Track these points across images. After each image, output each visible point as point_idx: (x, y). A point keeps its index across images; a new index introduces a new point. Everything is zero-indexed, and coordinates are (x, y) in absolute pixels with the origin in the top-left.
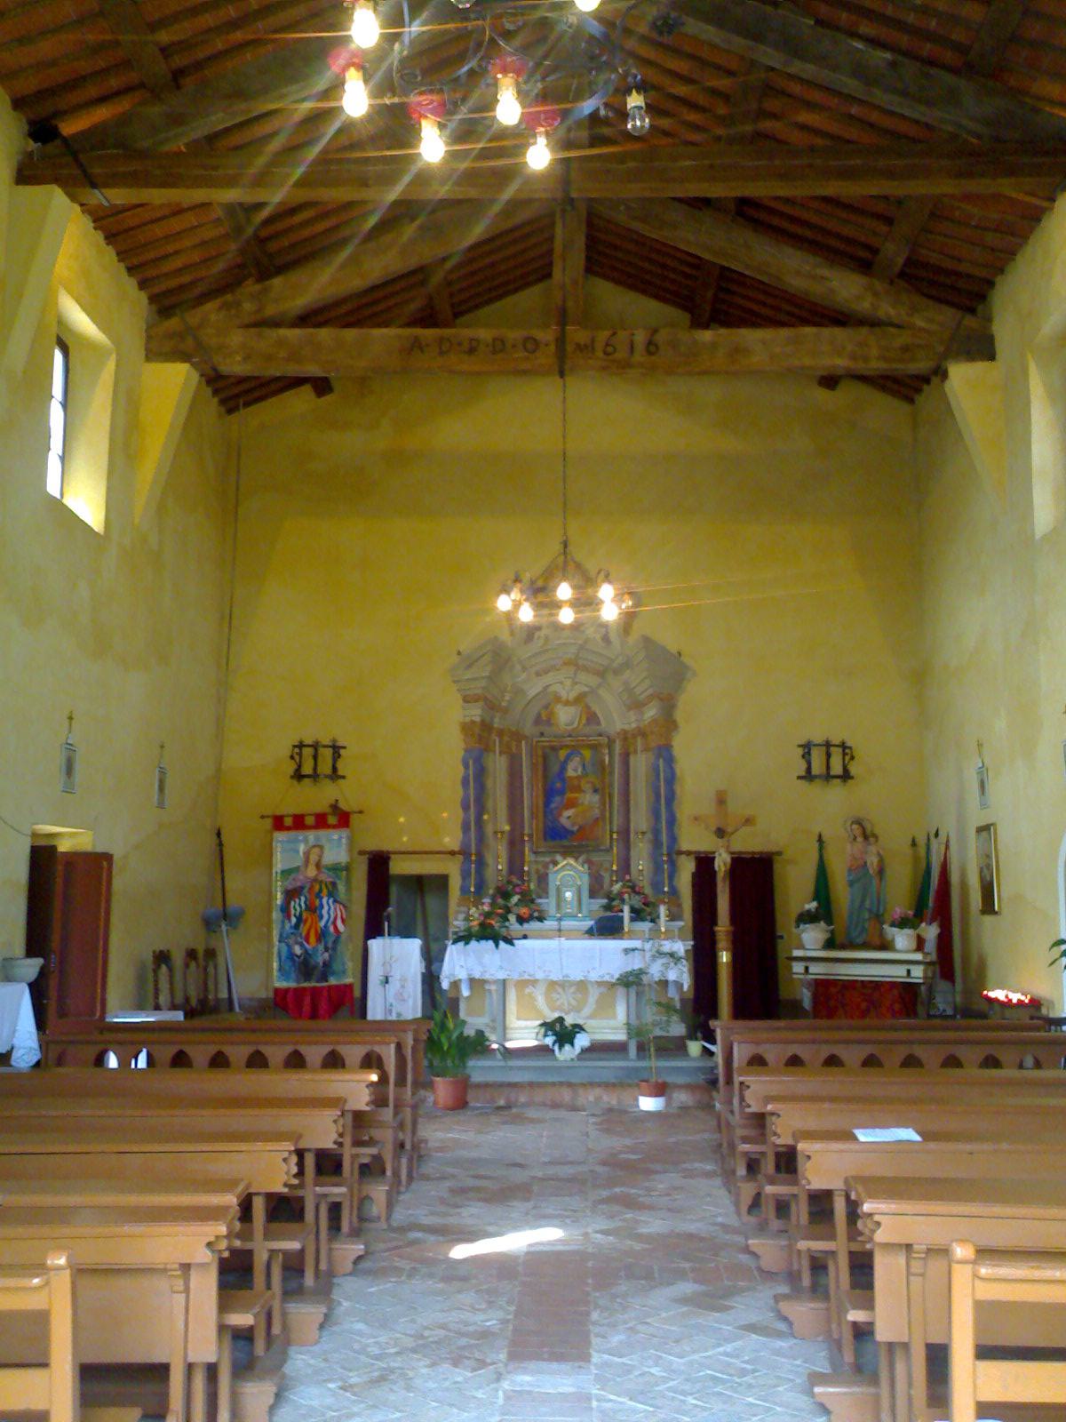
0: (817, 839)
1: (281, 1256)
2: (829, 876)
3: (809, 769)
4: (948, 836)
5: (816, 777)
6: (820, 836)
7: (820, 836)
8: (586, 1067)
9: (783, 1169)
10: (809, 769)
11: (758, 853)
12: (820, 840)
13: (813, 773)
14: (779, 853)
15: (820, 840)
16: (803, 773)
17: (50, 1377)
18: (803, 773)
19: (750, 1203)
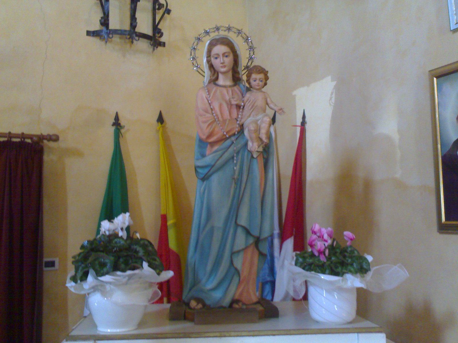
0: (113, 121)
1: (306, 269)
2: (124, 157)
3: (105, 22)
4: (304, 117)
5: (115, 32)
6: (117, 118)
7: (117, 118)
8: (438, 108)
9: (299, 264)
10: (105, 22)
11: (17, 136)
12: (117, 123)
13: (111, 27)
14: (55, 138)
15: (117, 123)
16: (96, 26)
17: (243, 38)
18: (96, 26)
19: (150, 298)
